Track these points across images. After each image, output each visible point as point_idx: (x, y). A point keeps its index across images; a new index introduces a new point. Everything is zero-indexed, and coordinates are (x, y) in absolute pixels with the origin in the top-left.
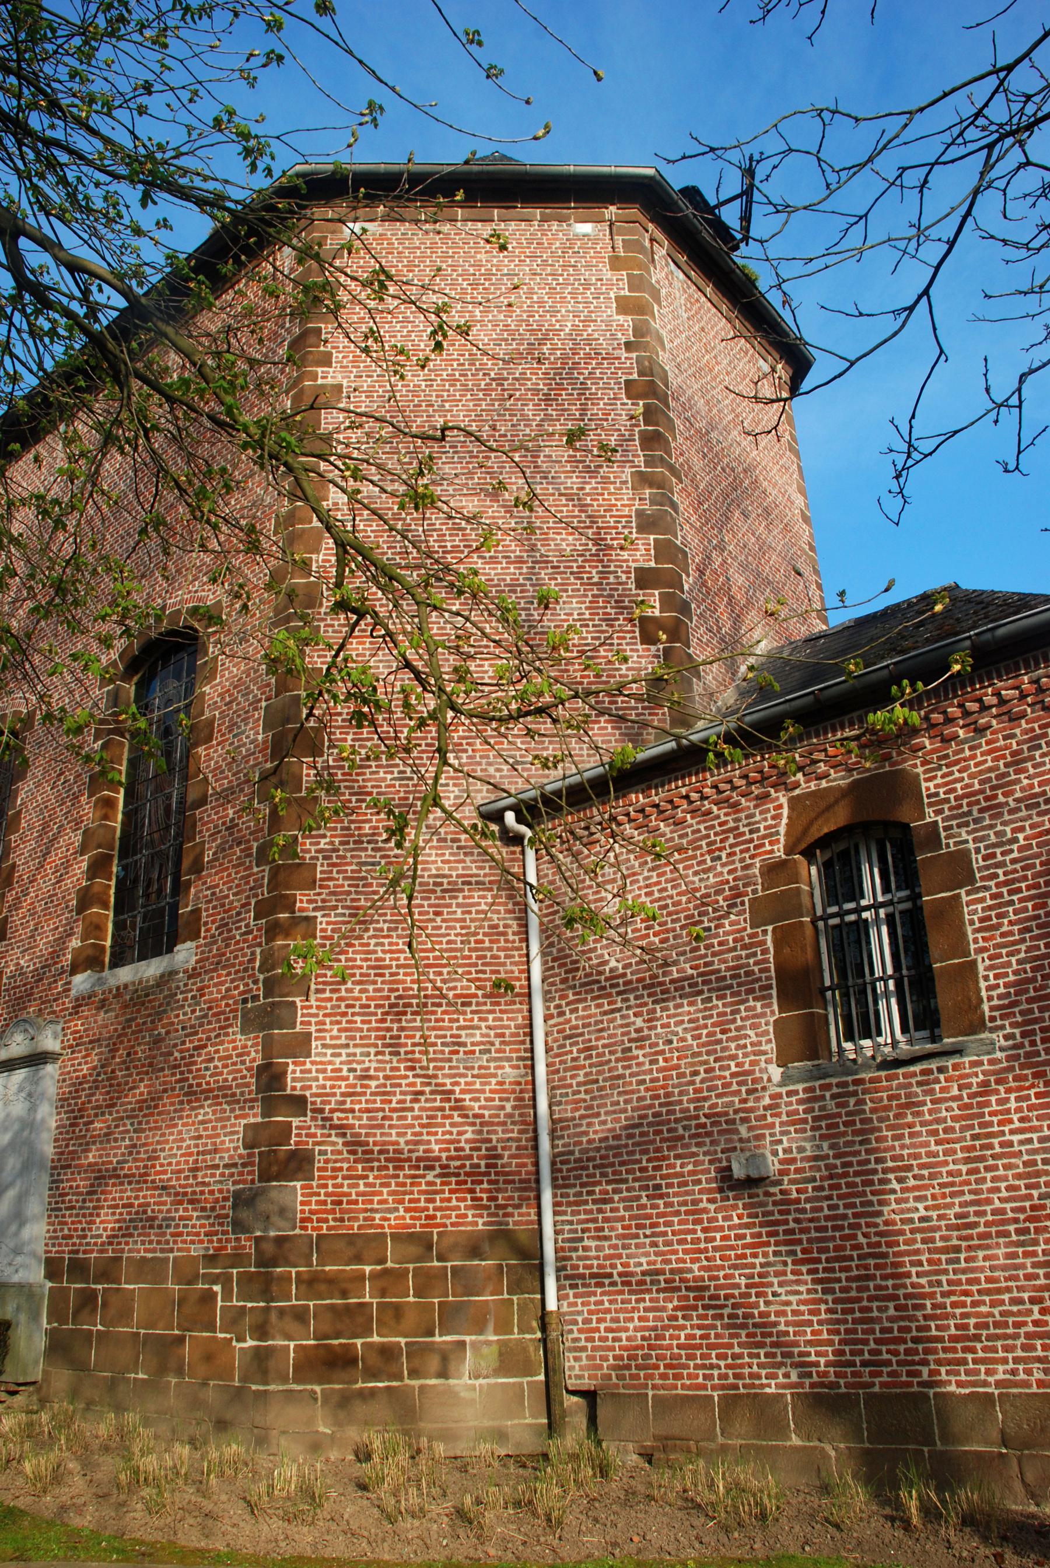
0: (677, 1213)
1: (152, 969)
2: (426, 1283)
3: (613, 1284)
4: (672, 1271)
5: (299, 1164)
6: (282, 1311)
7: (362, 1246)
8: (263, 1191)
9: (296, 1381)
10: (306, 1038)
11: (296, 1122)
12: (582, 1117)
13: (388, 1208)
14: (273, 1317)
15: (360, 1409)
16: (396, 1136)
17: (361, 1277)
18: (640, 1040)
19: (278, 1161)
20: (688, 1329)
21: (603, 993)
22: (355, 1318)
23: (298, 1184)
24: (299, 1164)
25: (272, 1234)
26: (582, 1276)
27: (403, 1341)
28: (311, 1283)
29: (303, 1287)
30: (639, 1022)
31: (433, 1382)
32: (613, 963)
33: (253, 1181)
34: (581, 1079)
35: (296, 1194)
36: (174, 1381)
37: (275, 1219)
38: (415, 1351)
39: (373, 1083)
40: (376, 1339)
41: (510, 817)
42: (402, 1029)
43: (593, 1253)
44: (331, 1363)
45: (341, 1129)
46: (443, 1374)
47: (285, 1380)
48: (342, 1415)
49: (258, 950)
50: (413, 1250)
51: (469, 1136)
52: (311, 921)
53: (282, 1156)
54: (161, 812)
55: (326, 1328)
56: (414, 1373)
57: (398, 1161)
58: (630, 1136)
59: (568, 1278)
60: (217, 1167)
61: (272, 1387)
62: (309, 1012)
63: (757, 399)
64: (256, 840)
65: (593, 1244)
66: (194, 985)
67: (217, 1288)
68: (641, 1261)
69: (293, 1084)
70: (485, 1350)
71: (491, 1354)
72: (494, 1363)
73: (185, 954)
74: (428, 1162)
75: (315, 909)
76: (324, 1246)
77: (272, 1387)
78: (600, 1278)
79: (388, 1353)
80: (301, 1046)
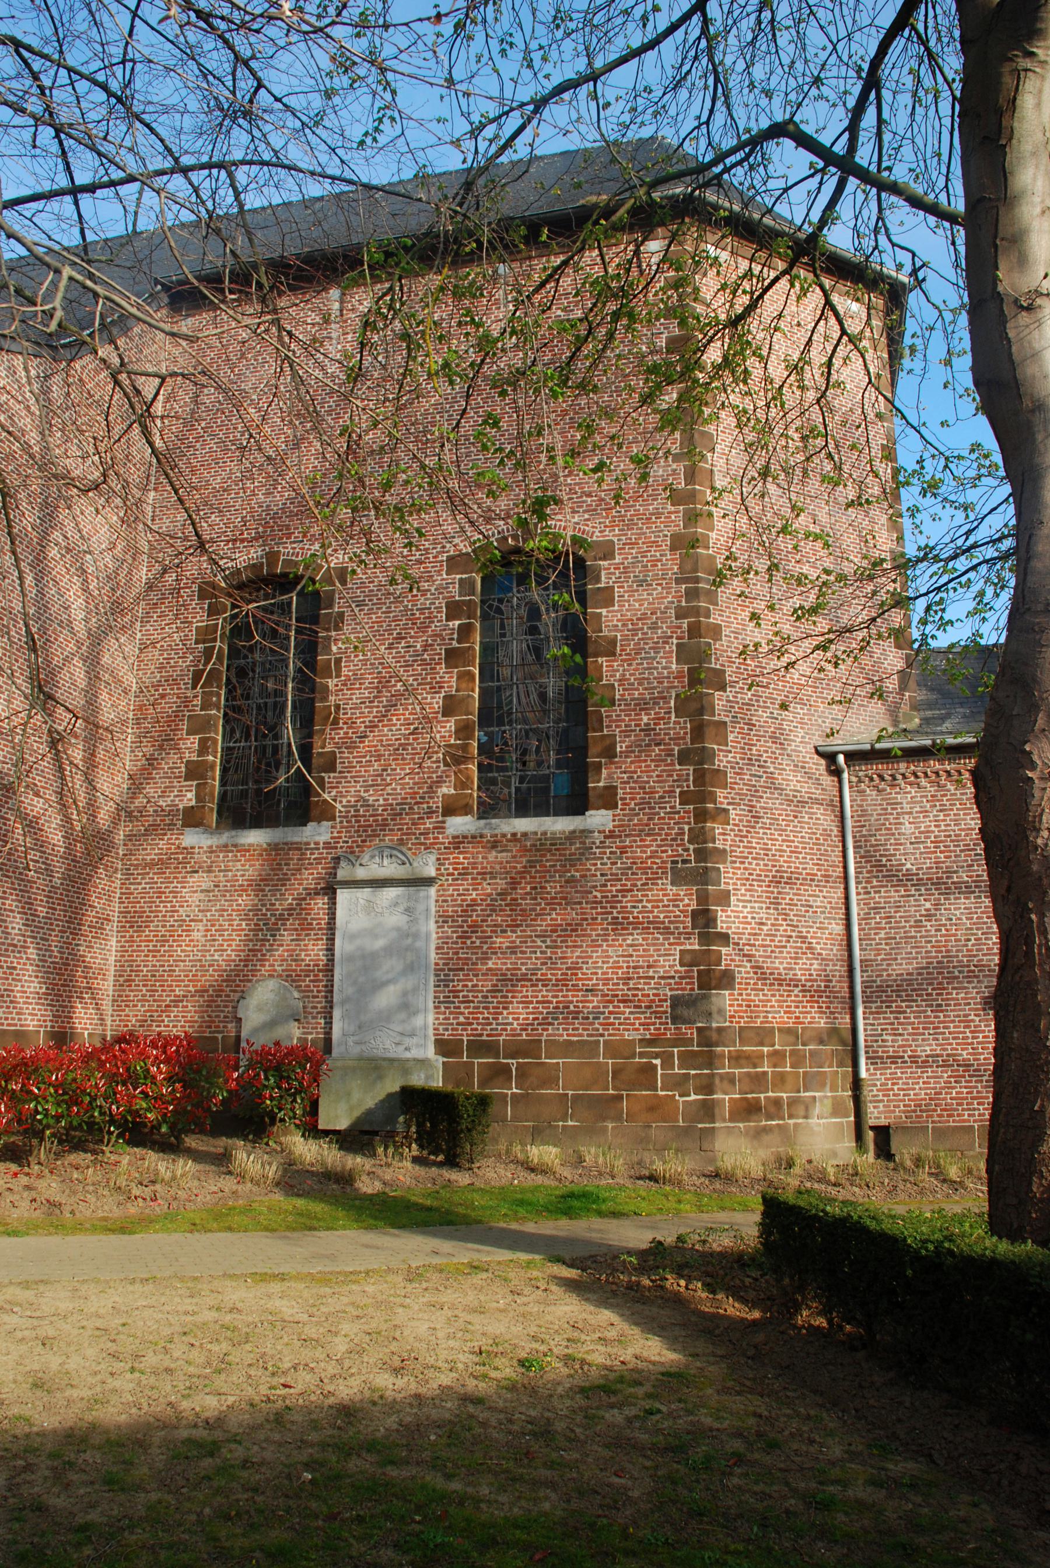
0: (953, 1021)
1: (561, 825)
2: (798, 1059)
3: (905, 1062)
4: (948, 1055)
5: (727, 980)
6: (721, 1075)
7: (764, 1035)
8: (705, 997)
9: (731, 1120)
10: (727, 894)
11: (724, 950)
12: (883, 960)
13: (777, 1011)
14: (717, 1081)
15: (766, 1138)
16: (780, 965)
17: (761, 1056)
18: (929, 916)
19: (711, 978)
20: (960, 1089)
21: (900, 883)
22: (759, 1081)
23: (727, 992)
24: (727, 980)
25: (714, 1025)
26: (882, 1058)
27: (784, 1095)
28: (737, 1059)
29: (733, 1062)
30: (928, 905)
31: (800, 1121)
32: (909, 866)
33: (692, 989)
34: (882, 936)
35: (725, 1000)
36: (610, 1126)
37: (715, 1016)
38: (793, 1102)
39: (765, 928)
40: (770, 1094)
41: (841, 758)
42: (779, 893)
43: (891, 1044)
44: (748, 1110)
45: (749, 957)
46: (806, 1117)
47: (724, 1120)
48: (755, 1143)
49: (686, 827)
50: (792, 1039)
51: (815, 966)
52: (726, 811)
53: (717, 974)
54: (534, 696)
55: (746, 1088)
56: (790, 1117)
57: (780, 981)
58: (919, 974)
59: (872, 1059)
60: (653, 978)
61: (717, 1125)
62: (729, 876)
63: (75, 191)
64: (678, 745)
65: (890, 1038)
66: (614, 845)
67: (657, 1062)
68: (927, 1048)
69: (721, 927)
70: (826, 1101)
71: (828, 1103)
72: (830, 1110)
73: (598, 819)
74: (794, 982)
75: (729, 804)
76: (744, 1035)
77: (717, 1125)
78: (894, 1059)
79: (777, 1102)
80: (724, 898)
